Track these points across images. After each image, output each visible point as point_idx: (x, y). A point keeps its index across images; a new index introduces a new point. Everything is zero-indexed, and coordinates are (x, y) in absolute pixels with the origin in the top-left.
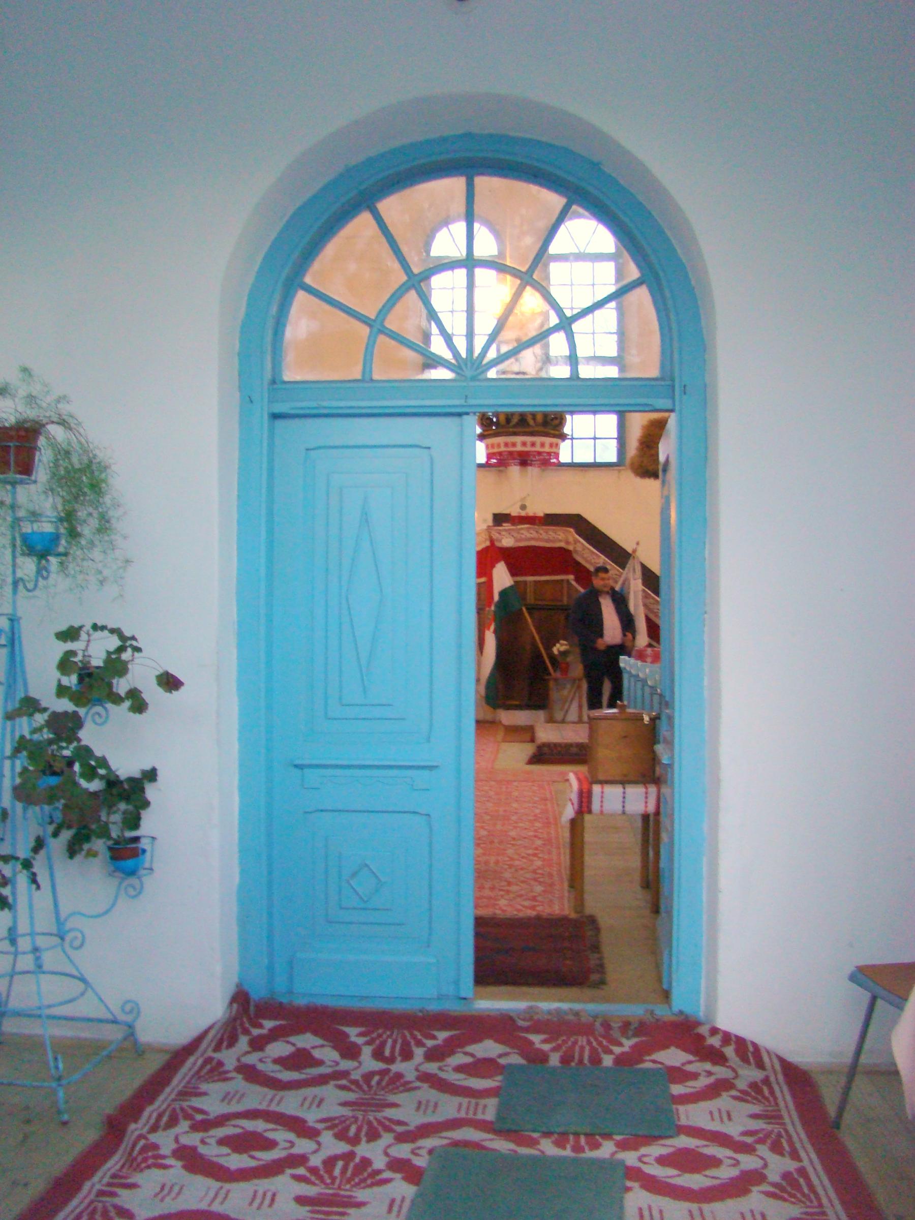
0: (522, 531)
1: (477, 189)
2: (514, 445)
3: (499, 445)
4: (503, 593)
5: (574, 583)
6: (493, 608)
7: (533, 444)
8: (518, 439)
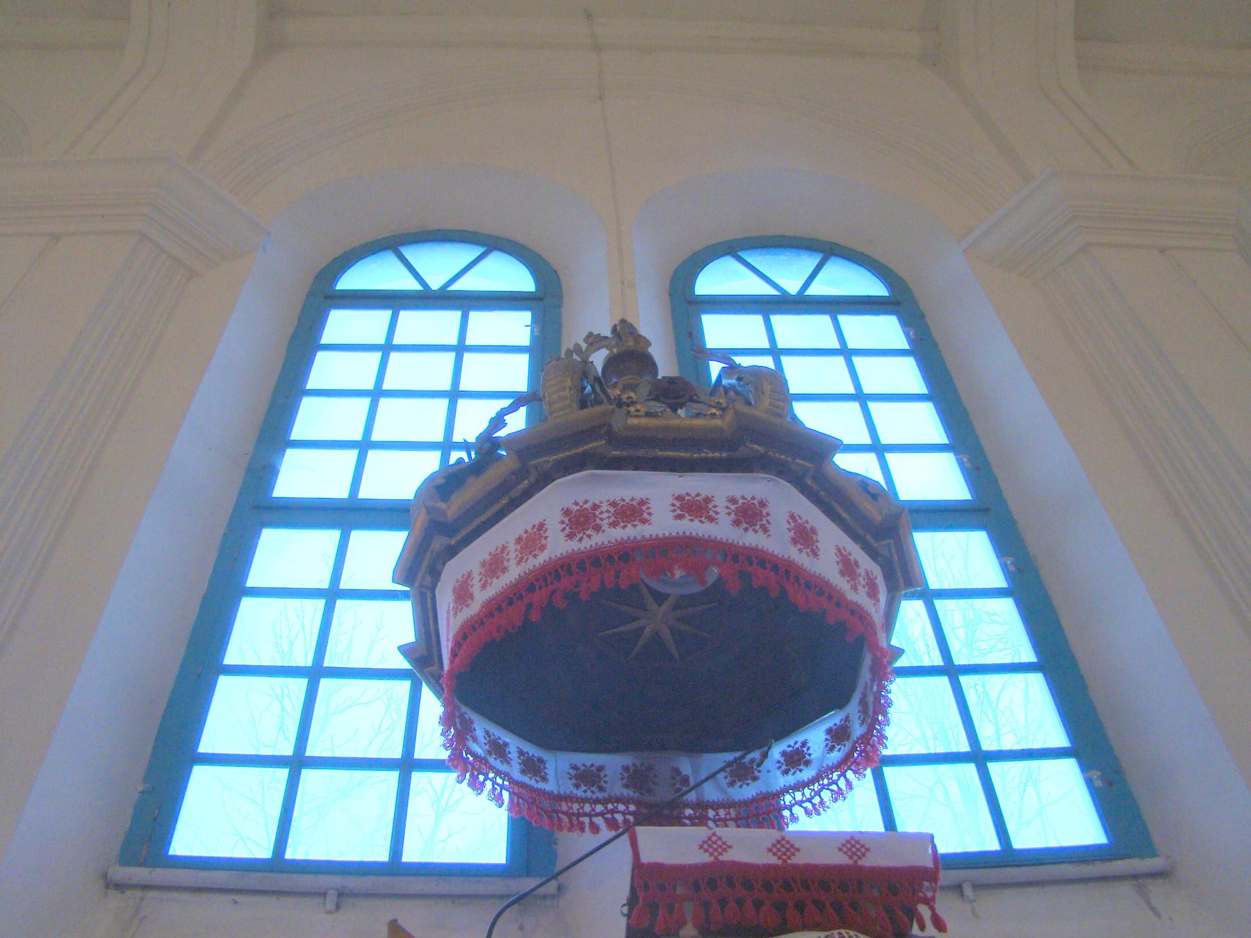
2: (631, 512)
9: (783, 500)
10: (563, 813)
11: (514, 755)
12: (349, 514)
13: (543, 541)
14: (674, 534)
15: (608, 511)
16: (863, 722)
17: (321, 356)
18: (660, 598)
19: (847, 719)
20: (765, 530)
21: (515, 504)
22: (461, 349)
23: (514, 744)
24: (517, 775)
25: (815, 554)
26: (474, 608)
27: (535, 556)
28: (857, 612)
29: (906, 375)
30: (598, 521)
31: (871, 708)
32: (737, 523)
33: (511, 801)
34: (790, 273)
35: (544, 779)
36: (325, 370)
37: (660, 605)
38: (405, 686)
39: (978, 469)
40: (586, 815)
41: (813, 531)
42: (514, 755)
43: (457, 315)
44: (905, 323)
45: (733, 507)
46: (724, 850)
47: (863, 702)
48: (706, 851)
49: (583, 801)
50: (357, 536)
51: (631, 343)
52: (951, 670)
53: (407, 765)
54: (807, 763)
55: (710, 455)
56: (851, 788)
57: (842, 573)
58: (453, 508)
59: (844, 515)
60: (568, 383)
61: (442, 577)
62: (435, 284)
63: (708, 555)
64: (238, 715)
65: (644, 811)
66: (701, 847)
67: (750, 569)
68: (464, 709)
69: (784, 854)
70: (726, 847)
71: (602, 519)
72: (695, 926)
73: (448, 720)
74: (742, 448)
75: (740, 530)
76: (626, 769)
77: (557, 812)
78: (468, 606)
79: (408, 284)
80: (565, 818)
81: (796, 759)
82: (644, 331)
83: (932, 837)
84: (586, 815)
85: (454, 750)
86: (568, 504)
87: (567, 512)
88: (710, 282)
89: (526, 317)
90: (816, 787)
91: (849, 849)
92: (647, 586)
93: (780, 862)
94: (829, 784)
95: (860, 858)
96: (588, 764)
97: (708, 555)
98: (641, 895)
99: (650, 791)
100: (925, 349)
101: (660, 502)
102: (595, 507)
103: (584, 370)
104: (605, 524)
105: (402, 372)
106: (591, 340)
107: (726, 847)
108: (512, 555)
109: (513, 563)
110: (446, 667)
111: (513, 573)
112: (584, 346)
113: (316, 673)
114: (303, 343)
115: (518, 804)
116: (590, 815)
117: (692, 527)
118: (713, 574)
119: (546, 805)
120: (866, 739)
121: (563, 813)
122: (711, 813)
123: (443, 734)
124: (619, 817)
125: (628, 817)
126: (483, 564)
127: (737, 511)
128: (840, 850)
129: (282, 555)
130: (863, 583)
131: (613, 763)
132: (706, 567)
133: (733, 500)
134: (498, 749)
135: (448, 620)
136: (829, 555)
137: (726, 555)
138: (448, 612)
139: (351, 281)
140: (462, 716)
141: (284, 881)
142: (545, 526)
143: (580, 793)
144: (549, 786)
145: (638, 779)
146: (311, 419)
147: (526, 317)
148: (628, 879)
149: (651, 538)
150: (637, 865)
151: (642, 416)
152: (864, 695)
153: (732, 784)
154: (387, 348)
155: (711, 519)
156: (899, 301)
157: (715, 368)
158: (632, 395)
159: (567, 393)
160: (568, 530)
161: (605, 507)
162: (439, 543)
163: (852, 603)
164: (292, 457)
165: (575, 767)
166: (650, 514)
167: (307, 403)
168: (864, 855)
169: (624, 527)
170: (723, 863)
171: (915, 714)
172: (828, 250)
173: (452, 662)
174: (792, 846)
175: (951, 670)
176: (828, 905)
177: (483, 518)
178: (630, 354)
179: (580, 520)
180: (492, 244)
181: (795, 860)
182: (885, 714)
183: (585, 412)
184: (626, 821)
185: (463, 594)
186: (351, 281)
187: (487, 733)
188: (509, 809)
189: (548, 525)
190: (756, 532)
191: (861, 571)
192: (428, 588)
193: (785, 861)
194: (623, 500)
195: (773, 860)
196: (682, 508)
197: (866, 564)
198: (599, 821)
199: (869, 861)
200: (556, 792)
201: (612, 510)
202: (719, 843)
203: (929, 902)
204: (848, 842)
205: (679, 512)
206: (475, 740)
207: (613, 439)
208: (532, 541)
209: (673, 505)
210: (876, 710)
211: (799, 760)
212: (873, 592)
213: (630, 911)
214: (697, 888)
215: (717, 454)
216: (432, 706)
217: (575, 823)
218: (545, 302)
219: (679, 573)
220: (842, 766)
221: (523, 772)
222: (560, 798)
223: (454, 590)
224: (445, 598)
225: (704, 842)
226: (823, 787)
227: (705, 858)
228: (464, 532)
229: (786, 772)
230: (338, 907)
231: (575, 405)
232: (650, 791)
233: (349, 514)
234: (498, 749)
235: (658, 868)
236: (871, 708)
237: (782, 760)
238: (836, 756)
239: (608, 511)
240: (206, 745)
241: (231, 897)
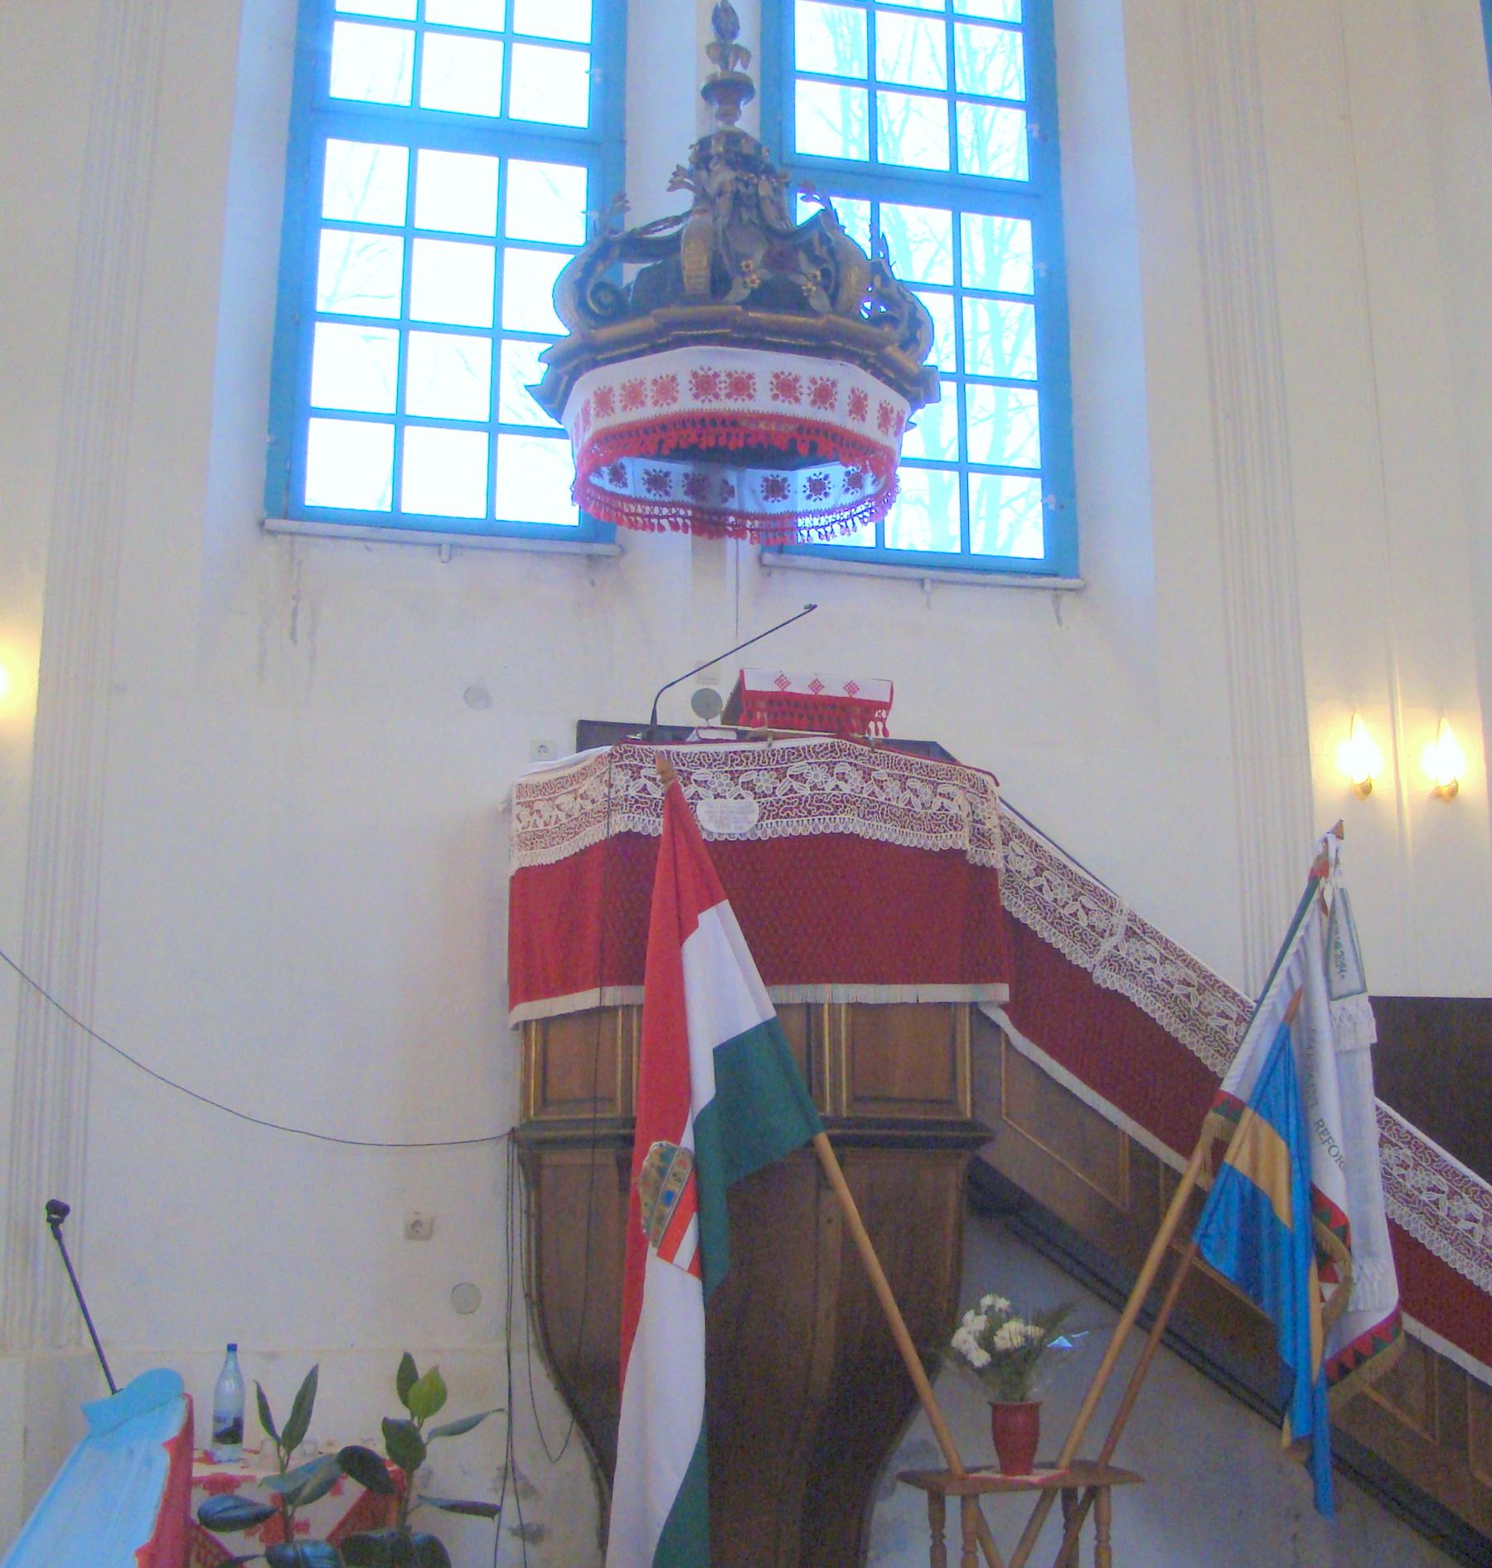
0: (795, 768)
1: (397, 303)
2: (741, 386)
3: (666, 388)
4: (729, 1056)
5: (1002, 1019)
6: (687, 1140)
7: (824, 394)
8: (763, 365)
35: (625, 485)
49: (653, 504)
64: (341, 367)
65: (699, 515)
76: (686, 476)
84: (656, 516)
86: (696, 368)
99: (704, 498)
102: (716, 375)
104: (723, 393)
116: (659, 517)
122: (749, 523)
124: (680, 521)
129: (355, 175)
131: (678, 471)
143: (650, 497)
145: (695, 486)
153: (766, 498)
161: (723, 377)
165: (647, 473)
184: (685, 525)
189: (679, 379)
195: (810, 692)
198: (664, 522)
227: (776, 689)
230: (450, 557)
232: (704, 498)
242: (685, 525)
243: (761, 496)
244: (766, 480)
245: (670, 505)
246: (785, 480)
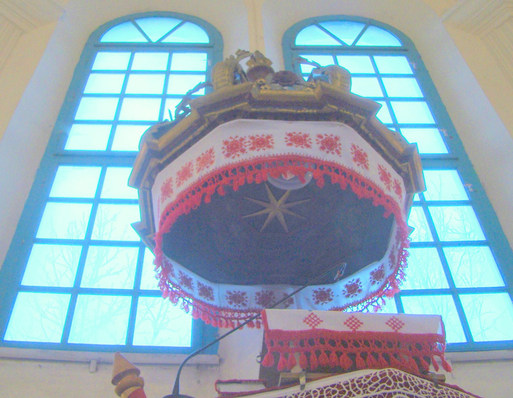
2: (261, 142)
9: (347, 137)
10: (222, 317)
11: (195, 285)
12: (106, 159)
13: (212, 159)
14: (287, 154)
15: (249, 142)
16: (391, 267)
17: (92, 76)
18: (278, 193)
19: (382, 266)
20: (338, 152)
21: (196, 139)
22: (168, 73)
23: (195, 279)
24: (197, 296)
25: (367, 167)
26: (173, 198)
27: (208, 167)
28: (389, 200)
29: (412, 88)
30: (243, 147)
31: (396, 259)
32: (323, 148)
33: (194, 310)
34: (348, 35)
35: (212, 299)
36: (94, 84)
37: (278, 200)
38: (136, 250)
39: (451, 137)
40: (235, 318)
41: (365, 155)
42: (195, 285)
43: (167, 55)
44: (410, 60)
45: (320, 140)
46: (318, 323)
47: (392, 257)
48: (308, 323)
50: (110, 170)
51: (261, 62)
52: (438, 245)
53: (136, 293)
54: (360, 291)
55: (307, 111)
56: (385, 304)
57: (382, 179)
58: (161, 143)
59: (383, 147)
60: (227, 72)
61: (155, 182)
62: (154, 39)
63: (306, 166)
64: (44, 265)
66: (305, 321)
67: (331, 174)
68: (167, 258)
69: (354, 325)
70: (319, 321)
71: (246, 146)
72: (302, 366)
73: (158, 262)
74: (326, 107)
75: (324, 152)
76: (258, 294)
77: (219, 317)
78: (169, 197)
79: (141, 39)
80: (224, 321)
81: (353, 289)
82: (267, 55)
83: (441, 317)
84: (235, 318)
85: (162, 279)
86: (227, 138)
87: (226, 143)
88: (304, 39)
89: (204, 56)
90: (365, 304)
91: (392, 324)
92: (270, 186)
93: (351, 330)
94: (372, 302)
95: (399, 328)
96: (237, 291)
97: (306, 166)
98: (269, 348)
100: (421, 74)
101: (279, 137)
102: (242, 139)
103: (236, 69)
105: (136, 84)
106: (239, 53)
107: (319, 321)
108: (195, 167)
109: (195, 171)
110: (157, 230)
111: (195, 177)
112: (236, 57)
113: (87, 243)
114: (83, 69)
115: (198, 312)
116: (237, 319)
117: (297, 150)
118: (309, 176)
119: (213, 312)
120: (392, 277)
121: (222, 317)
123: (155, 270)
125: (259, 320)
126: (178, 173)
127: (322, 142)
128: (387, 324)
129: (70, 181)
130: (393, 185)
132: (305, 172)
133: (320, 136)
134: (187, 282)
135: (158, 205)
136: (374, 168)
137: (316, 166)
138: (159, 201)
139: (108, 38)
140: (166, 262)
141: (66, 355)
142: (214, 151)
143: (232, 307)
144: (215, 303)
146: (86, 109)
147: (204, 56)
148: (261, 340)
149: (274, 156)
150: (267, 331)
151: (270, 90)
152: (392, 252)
154: (128, 72)
155: (308, 146)
156: (407, 49)
157: (306, 79)
158: (263, 80)
159: (226, 78)
160: (226, 153)
161: (247, 139)
162: (153, 163)
163: (387, 196)
164: (75, 128)
165: (229, 293)
166: (273, 143)
167: (84, 101)
168: (401, 327)
169: (258, 150)
170: (317, 330)
171: (420, 268)
172: (368, 23)
173: (160, 228)
174: (358, 321)
175: (438, 245)
176: (380, 355)
177: (178, 148)
178: (260, 68)
179: (233, 147)
180: (185, 19)
181: (359, 329)
182: (405, 261)
183: (236, 87)
184: (258, 323)
185: (167, 190)
186: (108, 38)
187: (180, 272)
188: (193, 314)
190: (333, 153)
191: (392, 179)
192: (147, 189)
193: (354, 329)
194: (258, 136)
195: (347, 329)
196: (291, 140)
197: (394, 175)
199: (404, 330)
200: (218, 306)
201: (252, 141)
202: (315, 319)
203: (439, 354)
204: (392, 319)
205: (289, 142)
206: (173, 275)
207: (252, 102)
208: (206, 159)
209: (286, 138)
210: (399, 260)
211: (356, 289)
212: (398, 190)
213: (262, 360)
214: (302, 344)
215: (311, 111)
216: (150, 256)
217: (229, 323)
218: (213, 48)
219: (290, 176)
220: (379, 293)
221: (200, 294)
222: (221, 309)
223: (162, 189)
224: (157, 193)
225: (306, 318)
226: (369, 303)
227: (307, 327)
228: (168, 156)
229: (348, 296)
230: (97, 370)
231: (230, 84)
233: (106, 159)
234: (187, 282)
235: (279, 333)
236: (396, 259)
237: (346, 290)
238: (375, 288)
239: (249, 142)
240: (25, 282)
241: (37, 364)
242: (258, 323)
243: (313, 302)
244: (316, 292)
245: (246, 312)
246: (329, 290)
